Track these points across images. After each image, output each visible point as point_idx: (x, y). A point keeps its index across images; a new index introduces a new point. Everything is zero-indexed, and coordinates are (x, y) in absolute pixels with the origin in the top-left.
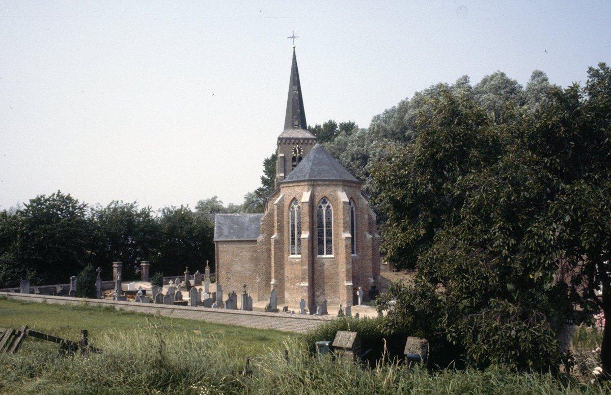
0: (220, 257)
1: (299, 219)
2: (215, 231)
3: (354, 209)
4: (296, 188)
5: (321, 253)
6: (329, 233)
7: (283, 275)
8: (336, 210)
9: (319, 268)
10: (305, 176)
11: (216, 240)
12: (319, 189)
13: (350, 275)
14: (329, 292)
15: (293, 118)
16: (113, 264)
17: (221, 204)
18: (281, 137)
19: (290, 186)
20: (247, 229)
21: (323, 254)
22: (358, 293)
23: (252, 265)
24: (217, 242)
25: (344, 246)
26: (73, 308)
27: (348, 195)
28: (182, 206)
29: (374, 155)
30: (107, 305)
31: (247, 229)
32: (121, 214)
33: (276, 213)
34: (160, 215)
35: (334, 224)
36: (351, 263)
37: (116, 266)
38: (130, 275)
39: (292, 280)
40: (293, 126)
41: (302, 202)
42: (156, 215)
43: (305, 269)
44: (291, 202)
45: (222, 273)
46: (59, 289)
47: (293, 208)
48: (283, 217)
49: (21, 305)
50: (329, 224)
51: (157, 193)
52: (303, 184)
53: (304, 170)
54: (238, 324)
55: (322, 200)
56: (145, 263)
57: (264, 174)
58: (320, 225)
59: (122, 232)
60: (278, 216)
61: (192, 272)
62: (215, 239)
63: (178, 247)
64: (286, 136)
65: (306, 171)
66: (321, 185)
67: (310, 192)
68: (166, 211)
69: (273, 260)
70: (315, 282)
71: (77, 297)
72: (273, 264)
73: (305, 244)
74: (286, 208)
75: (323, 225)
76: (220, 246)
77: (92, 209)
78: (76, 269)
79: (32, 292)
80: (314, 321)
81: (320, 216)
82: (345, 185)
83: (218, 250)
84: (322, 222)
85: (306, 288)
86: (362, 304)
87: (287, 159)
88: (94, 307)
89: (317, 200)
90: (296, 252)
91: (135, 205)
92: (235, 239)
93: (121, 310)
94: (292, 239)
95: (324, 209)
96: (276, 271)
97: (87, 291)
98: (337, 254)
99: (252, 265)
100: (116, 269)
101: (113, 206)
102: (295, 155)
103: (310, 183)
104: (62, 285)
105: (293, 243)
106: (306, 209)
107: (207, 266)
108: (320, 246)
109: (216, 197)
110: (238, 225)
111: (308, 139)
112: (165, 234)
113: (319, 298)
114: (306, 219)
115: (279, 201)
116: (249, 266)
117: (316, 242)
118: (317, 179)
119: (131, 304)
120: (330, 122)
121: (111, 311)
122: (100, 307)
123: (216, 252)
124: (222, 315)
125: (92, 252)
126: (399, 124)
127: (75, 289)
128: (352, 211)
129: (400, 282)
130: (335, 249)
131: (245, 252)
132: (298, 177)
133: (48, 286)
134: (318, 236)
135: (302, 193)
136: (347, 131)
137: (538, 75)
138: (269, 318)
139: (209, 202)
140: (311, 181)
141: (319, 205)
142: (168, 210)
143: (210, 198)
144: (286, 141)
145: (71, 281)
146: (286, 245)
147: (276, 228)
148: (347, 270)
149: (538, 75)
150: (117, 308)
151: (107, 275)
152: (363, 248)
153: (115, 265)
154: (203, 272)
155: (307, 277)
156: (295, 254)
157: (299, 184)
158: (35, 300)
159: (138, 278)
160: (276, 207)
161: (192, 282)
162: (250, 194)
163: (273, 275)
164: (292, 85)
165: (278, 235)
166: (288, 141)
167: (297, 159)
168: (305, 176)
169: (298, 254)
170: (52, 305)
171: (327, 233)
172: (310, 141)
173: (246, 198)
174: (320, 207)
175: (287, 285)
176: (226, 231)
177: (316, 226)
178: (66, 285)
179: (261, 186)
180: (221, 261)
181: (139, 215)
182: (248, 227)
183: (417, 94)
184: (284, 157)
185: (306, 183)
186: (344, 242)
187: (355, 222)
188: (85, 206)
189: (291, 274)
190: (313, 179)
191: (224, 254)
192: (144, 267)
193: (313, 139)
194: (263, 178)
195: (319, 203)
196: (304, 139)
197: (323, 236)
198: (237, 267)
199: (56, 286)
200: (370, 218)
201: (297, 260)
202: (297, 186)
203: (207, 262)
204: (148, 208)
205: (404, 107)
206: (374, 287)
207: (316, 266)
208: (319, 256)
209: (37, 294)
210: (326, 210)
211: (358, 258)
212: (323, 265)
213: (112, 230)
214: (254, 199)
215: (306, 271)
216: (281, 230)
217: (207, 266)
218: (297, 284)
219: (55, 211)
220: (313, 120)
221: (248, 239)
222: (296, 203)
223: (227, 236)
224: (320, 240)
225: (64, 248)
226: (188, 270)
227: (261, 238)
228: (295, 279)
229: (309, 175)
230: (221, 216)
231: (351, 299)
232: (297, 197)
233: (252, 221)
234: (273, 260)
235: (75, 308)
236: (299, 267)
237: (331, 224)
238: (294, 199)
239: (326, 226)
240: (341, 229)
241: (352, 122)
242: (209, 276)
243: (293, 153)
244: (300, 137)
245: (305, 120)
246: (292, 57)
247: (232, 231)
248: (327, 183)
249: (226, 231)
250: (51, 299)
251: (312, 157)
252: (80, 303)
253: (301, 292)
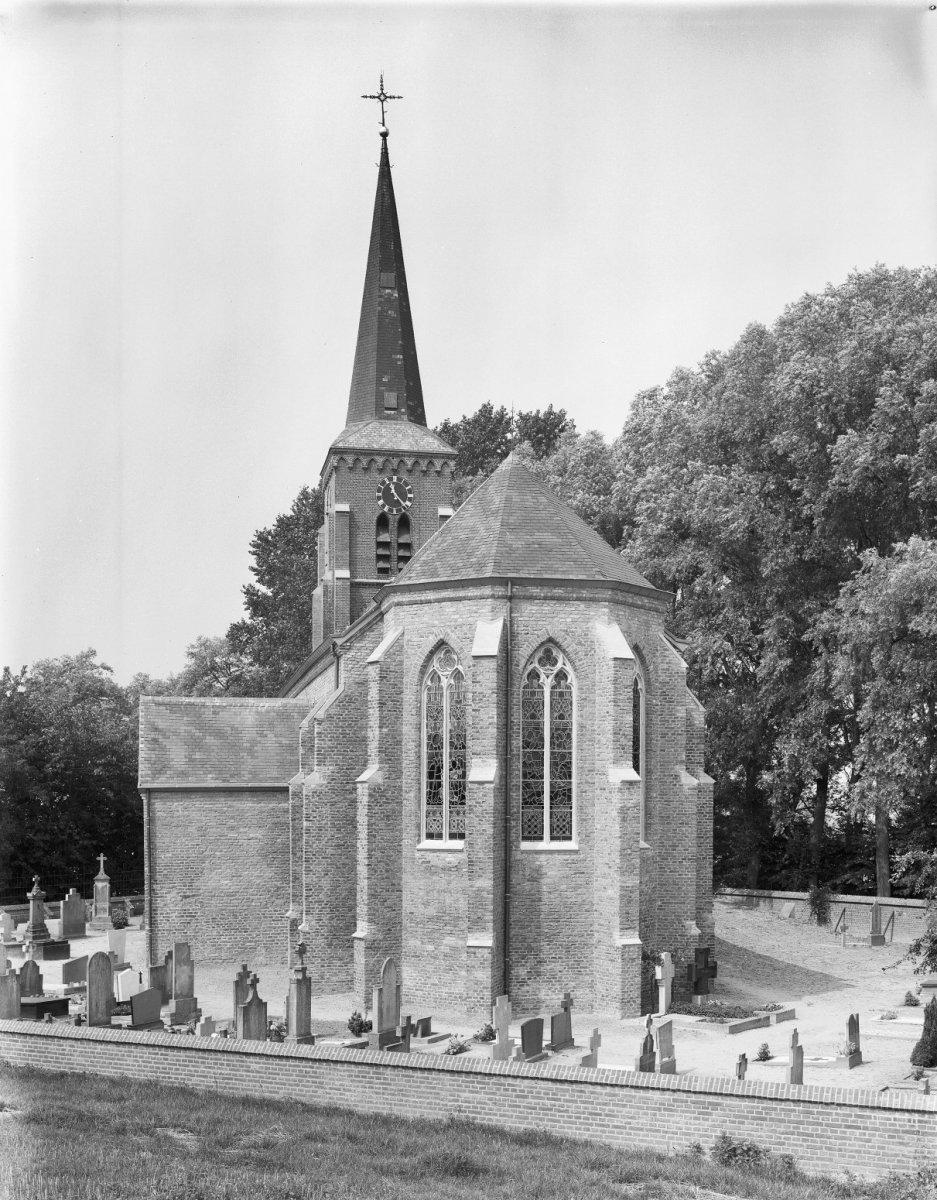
0: (159, 842)
1: (458, 715)
2: (142, 755)
6: (562, 767)
7: (396, 908)
8: (588, 691)
9: (527, 886)
11: (148, 786)
12: (528, 612)
13: (635, 910)
14: (557, 966)
15: (379, 382)
17: (105, 675)
18: (340, 445)
20: (251, 752)
21: (541, 839)
22: (659, 972)
23: (269, 873)
24: (149, 791)
25: (615, 813)
27: (627, 633)
29: (652, 515)
31: (251, 752)
35: (581, 735)
36: (637, 871)
39: (431, 926)
40: (381, 412)
43: (480, 890)
45: (168, 900)
47: (435, 677)
50: (562, 735)
52: (472, 592)
53: (473, 543)
54: (322, 1099)
55: (540, 654)
57: (252, 579)
58: (533, 739)
60: (382, 704)
67: (499, 624)
72: (362, 870)
73: (483, 803)
74: (410, 678)
75: (542, 739)
76: (158, 805)
80: (633, 1092)
81: (533, 709)
82: (617, 602)
83: (151, 821)
84: (539, 729)
86: (670, 1010)
87: (359, 518)
89: (523, 652)
90: (446, 832)
92: (211, 782)
94: (430, 785)
95: (547, 682)
98: (586, 838)
99: (269, 873)
102: (386, 509)
103: (500, 590)
105: (434, 797)
106: (488, 678)
107: (102, 874)
108: (531, 811)
109: (94, 653)
110: (219, 734)
111: (431, 457)
113: (526, 988)
114: (487, 717)
115: (388, 654)
116: (261, 875)
117: (517, 797)
118: (522, 575)
120: (486, 410)
124: (254, 1064)
126: (741, 412)
128: (636, 692)
129: (22, 839)
130: (582, 820)
131: (250, 824)
132: (455, 570)
135: (472, 627)
136: (536, 444)
138: (448, 1076)
139: (68, 666)
141: (530, 668)
143: (74, 653)
144: (357, 460)
146: (409, 806)
147: (373, 747)
148: (626, 897)
152: (665, 819)
154: (87, 892)
155: (489, 917)
156: (440, 836)
157: (461, 593)
160: (373, 672)
161: (54, 927)
162: (205, 644)
163: (362, 909)
165: (380, 769)
166: (364, 462)
167: (393, 524)
168: (481, 566)
169: (452, 836)
171: (554, 765)
172: (438, 464)
173: (192, 655)
174: (534, 675)
175: (411, 943)
176: (178, 755)
177: (517, 742)
179: (243, 615)
180: (163, 858)
182: (254, 743)
183: (550, 413)
184: (350, 515)
185: (487, 591)
186: (616, 798)
189: (426, 904)
191: (174, 833)
193: (448, 456)
194: (250, 592)
195: (530, 660)
196: (419, 456)
197: (542, 777)
198: (217, 880)
201: (451, 858)
203: (102, 858)
207: (515, 879)
208: (526, 845)
210: (553, 687)
211: (650, 853)
212: (536, 876)
214: (217, 660)
215: (485, 894)
216: (390, 753)
217: (102, 874)
218: (449, 940)
220: (449, 399)
221: (256, 785)
222: (448, 661)
223: (183, 774)
224: (536, 793)
227: (313, 779)
228: (444, 921)
229: (497, 564)
230: (158, 704)
231: (636, 993)
232: (453, 643)
233: (266, 723)
234: (362, 855)
236: (459, 882)
237: (569, 736)
238: (441, 644)
240: (608, 753)
241: (556, 410)
242: (106, 905)
243: (381, 502)
244: (404, 447)
246: (377, 171)
247: (198, 756)
248: (558, 592)
249: (178, 755)
251: (497, 500)
253: (469, 969)
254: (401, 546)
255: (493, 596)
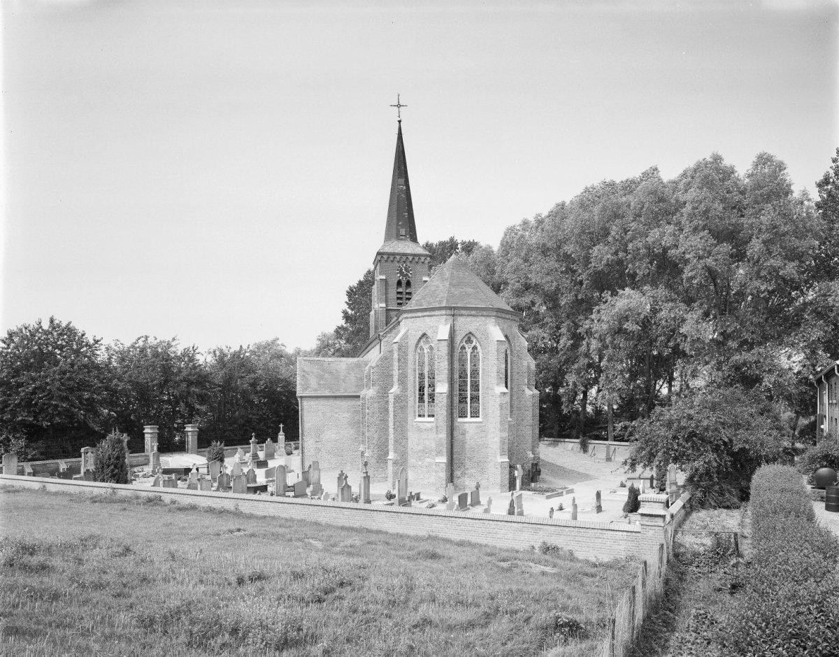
1: (431, 365)
3: (508, 352)
4: (427, 319)
5: (463, 415)
6: (475, 387)
9: (461, 437)
10: (441, 302)
12: (461, 321)
13: (506, 447)
15: (398, 225)
16: (144, 429)
17: (283, 348)
19: (419, 317)
21: (466, 417)
22: (516, 473)
24: (301, 397)
26: (91, 498)
27: (502, 330)
28: (241, 347)
30: (150, 495)
32: (153, 356)
33: (396, 356)
34: (210, 359)
37: (149, 431)
38: (168, 445)
40: (398, 237)
41: (438, 340)
42: (205, 359)
44: (419, 341)
46: (63, 465)
47: (422, 349)
48: (406, 362)
49: (4, 493)
50: (475, 373)
51: (208, 328)
54: (374, 527)
55: (466, 339)
56: (192, 427)
57: (346, 307)
58: (463, 375)
59: (155, 382)
61: (261, 441)
62: (298, 395)
63: (247, 407)
64: (388, 249)
65: (442, 295)
66: (464, 315)
68: (218, 353)
69: (391, 424)
70: (454, 457)
71: (95, 480)
77: (107, 349)
78: (93, 438)
79: (21, 472)
80: (506, 523)
81: (462, 362)
85: (444, 466)
86: (521, 489)
88: (126, 497)
89: (458, 339)
90: (426, 414)
91: (173, 344)
93: (173, 502)
95: (469, 351)
96: (396, 441)
97: (113, 471)
100: (149, 436)
101: (141, 343)
103: (449, 312)
104: (69, 460)
105: (421, 399)
106: (444, 349)
108: (462, 405)
110: (331, 373)
111: (419, 256)
112: (219, 386)
114: (442, 368)
115: (401, 339)
116: (349, 432)
117: (456, 399)
119: (181, 493)
121: (156, 504)
122: (137, 498)
123: (300, 412)
125: (110, 411)
127: (92, 468)
130: (484, 409)
133: (47, 462)
134: (460, 390)
137: (764, 160)
138: (428, 517)
140: (450, 308)
141: (461, 345)
142: (221, 351)
144: (388, 258)
145: (83, 455)
146: (410, 403)
147: (395, 378)
149: (764, 160)
150: (167, 499)
151: (137, 445)
152: (519, 409)
153: (148, 430)
154: (275, 440)
155: (445, 450)
156: (424, 416)
158: (27, 485)
159: (181, 448)
160: (395, 346)
163: (391, 447)
164: (396, 177)
166: (392, 258)
168: (441, 302)
170: (56, 494)
171: (472, 386)
174: (463, 348)
175: (412, 461)
176: (313, 382)
177: (456, 376)
178: (74, 460)
181: (179, 359)
182: (346, 377)
184: (386, 280)
187: (509, 367)
188: (96, 342)
190: (453, 306)
191: (311, 415)
192: (190, 434)
194: (345, 312)
198: (330, 435)
199: (59, 461)
200: (529, 367)
202: (428, 316)
203: (281, 426)
204: (193, 348)
205: (560, 212)
206: (535, 465)
207: (456, 434)
209: (29, 474)
213: (141, 379)
214: (330, 342)
216: (403, 381)
219: (50, 348)
222: (427, 342)
223: (316, 390)
224: (464, 397)
225: (61, 406)
226: (256, 437)
228: (425, 452)
230: (305, 360)
231: (507, 482)
232: (429, 334)
233: (350, 368)
234: (391, 424)
235: (94, 500)
238: (424, 335)
239: (471, 377)
240: (495, 381)
242: (283, 445)
243: (398, 275)
244: (409, 252)
245: (415, 229)
246: (397, 136)
248: (473, 312)
249: (313, 382)
250: (55, 485)
252: (103, 491)
254: (407, 293)
255: (446, 314)
